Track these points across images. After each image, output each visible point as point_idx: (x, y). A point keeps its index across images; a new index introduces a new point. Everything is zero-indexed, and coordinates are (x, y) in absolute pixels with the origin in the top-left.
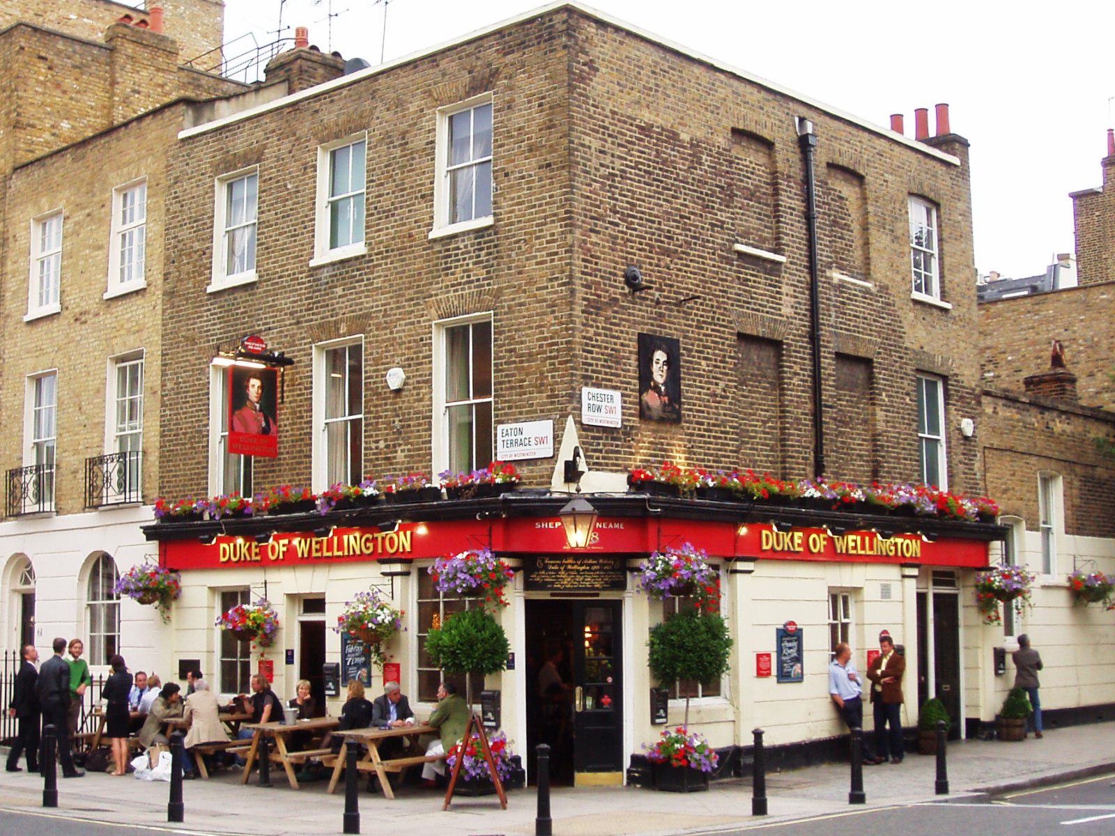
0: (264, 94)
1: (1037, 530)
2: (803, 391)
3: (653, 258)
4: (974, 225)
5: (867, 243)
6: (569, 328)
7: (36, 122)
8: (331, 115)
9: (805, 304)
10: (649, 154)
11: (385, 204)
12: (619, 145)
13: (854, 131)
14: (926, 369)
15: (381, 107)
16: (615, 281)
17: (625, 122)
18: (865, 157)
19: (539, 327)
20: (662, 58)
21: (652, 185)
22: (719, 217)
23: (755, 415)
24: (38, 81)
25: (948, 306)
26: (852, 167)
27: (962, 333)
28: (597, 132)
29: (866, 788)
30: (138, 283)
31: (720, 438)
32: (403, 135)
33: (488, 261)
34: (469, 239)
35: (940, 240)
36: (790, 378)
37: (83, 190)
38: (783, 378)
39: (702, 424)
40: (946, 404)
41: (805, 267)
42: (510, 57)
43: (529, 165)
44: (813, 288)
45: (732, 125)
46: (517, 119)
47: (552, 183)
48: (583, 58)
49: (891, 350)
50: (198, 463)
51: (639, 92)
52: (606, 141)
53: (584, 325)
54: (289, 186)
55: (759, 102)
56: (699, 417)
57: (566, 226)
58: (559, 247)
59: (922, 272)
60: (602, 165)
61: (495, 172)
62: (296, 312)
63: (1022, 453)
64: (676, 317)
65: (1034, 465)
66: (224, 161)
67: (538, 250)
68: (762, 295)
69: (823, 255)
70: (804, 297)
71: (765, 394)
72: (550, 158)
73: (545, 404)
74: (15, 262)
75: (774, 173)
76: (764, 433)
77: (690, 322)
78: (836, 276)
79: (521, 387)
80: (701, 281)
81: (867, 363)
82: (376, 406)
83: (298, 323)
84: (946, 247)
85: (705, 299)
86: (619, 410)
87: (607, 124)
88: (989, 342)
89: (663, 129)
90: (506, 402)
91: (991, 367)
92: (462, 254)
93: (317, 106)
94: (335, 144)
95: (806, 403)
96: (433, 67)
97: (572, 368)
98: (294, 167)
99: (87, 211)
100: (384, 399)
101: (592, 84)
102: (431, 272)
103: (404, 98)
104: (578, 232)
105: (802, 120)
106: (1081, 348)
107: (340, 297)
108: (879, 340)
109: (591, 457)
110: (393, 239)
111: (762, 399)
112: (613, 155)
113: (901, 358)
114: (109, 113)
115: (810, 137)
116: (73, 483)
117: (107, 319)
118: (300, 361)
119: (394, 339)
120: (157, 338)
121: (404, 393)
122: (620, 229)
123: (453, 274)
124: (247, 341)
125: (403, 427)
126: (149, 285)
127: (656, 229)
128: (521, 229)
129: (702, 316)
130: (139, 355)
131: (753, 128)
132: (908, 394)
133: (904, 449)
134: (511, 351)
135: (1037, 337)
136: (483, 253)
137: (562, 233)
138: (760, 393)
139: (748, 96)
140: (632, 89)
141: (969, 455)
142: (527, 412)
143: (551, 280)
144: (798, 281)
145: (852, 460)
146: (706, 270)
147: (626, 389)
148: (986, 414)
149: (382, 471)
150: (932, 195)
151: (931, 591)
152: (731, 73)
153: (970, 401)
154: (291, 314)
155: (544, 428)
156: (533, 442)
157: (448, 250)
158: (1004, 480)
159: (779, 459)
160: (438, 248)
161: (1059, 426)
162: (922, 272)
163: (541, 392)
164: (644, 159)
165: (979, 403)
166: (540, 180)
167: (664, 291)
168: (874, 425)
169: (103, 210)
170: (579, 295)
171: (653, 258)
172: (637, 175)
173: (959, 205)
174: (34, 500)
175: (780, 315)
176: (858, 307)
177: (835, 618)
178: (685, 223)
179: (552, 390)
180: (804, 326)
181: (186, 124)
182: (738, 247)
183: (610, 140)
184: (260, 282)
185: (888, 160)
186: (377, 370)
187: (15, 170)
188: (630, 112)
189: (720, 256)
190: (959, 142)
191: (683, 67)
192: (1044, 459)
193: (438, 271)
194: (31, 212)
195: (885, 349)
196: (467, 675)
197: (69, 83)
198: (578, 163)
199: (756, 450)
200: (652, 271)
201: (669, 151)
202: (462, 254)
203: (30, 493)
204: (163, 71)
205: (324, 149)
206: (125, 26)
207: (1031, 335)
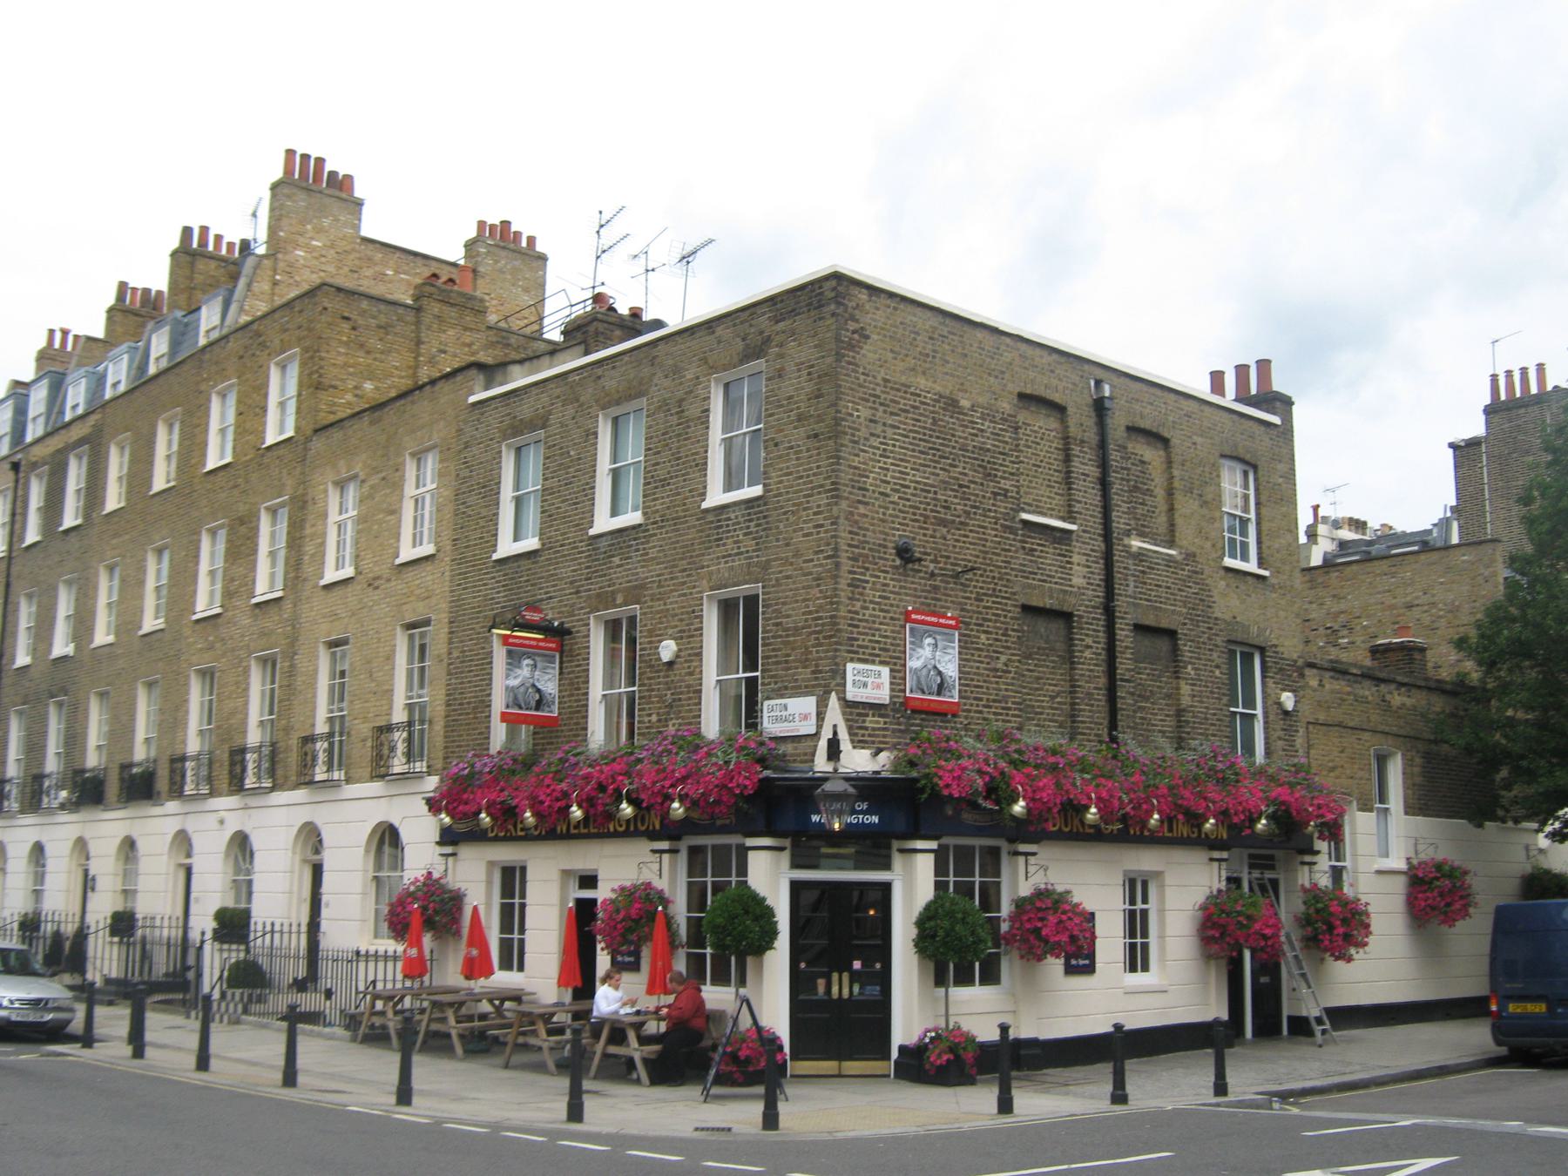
0: (560, 356)
1: (1371, 810)
2: (1096, 665)
4: (1298, 487)
5: (1171, 509)
6: (833, 603)
7: (338, 383)
8: (612, 381)
10: (925, 422)
11: (661, 473)
15: (660, 374)
17: (898, 390)
18: (1171, 418)
23: (1041, 689)
24: (340, 341)
25: (1266, 573)
26: (1155, 430)
27: (1283, 602)
28: (868, 401)
29: (1129, 1089)
30: (427, 549)
31: (1001, 714)
32: (681, 401)
33: (757, 532)
34: (740, 510)
35: (1258, 504)
38: (1074, 651)
39: (981, 699)
40: (1264, 677)
41: (1099, 535)
43: (797, 435)
45: (1018, 390)
46: (787, 387)
47: (819, 454)
48: (852, 326)
50: (480, 734)
52: (876, 409)
53: (850, 599)
54: (572, 453)
57: (832, 497)
58: (825, 519)
59: (1238, 537)
61: (765, 441)
63: (1352, 728)
64: (952, 589)
66: (512, 427)
67: (805, 522)
69: (1120, 521)
70: (1099, 567)
73: (809, 680)
74: (313, 526)
75: (1066, 439)
76: (1052, 708)
78: (1136, 543)
81: (1171, 634)
82: (650, 678)
83: (577, 592)
84: (1264, 511)
85: (985, 571)
86: (887, 686)
87: (878, 393)
88: (1343, 606)
89: (941, 396)
90: (772, 677)
91: (1345, 632)
92: (734, 524)
93: (599, 372)
94: (518, 440)
97: (836, 643)
99: (383, 474)
100: (657, 672)
101: (863, 352)
102: (704, 543)
104: (844, 504)
105: (1098, 383)
109: (856, 735)
110: (668, 508)
111: (1051, 673)
112: (884, 424)
113: (1210, 628)
114: (415, 373)
115: (1106, 401)
116: (362, 752)
117: (397, 586)
118: (578, 632)
120: (444, 606)
121: (676, 666)
123: (724, 545)
124: (526, 610)
125: (674, 700)
126: (438, 551)
129: (982, 588)
130: (427, 623)
131: (1040, 391)
132: (1218, 667)
134: (777, 624)
136: (752, 524)
137: (828, 504)
139: (1037, 359)
140: (907, 355)
141: (1290, 731)
142: (793, 688)
143: (817, 553)
144: (1092, 550)
146: (986, 540)
147: (895, 664)
148: (1311, 687)
150: (1248, 457)
152: (1017, 336)
153: (1290, 673)
154: (572, 583)
155: (808, 704)
156: (797, 719)
157: (719, 521)
158: (1331, 757)
161: (1397, 699)
162: (1238, 537)
163: (805, 667)
165: (1302, 675)
166: (808, 450)
167: (939, 562)
168: (1179, 700)
169: (397, 474)
170: (845, 568)
173: (1279, 466)
174: (404, 760)
177: (1133, 902)
178: (964, 493)
179: (817, 666)
181: (477, 388)
182: (1025, 516)
183: (881, 408)
186: (650, 642)
187: (316, 431)
189: (1002, 525)
190: (1281, 401)
192: (1379, 735)
193: (710, 541)
194: (331, 476)
195: (1192, 620)
196: (733, 958)
197: (374, 343)
198: (846, 434)
201: (947, 418)
202: (734, 524)
203: (320, 761)
205: (605, 416)
206: (433, 286)
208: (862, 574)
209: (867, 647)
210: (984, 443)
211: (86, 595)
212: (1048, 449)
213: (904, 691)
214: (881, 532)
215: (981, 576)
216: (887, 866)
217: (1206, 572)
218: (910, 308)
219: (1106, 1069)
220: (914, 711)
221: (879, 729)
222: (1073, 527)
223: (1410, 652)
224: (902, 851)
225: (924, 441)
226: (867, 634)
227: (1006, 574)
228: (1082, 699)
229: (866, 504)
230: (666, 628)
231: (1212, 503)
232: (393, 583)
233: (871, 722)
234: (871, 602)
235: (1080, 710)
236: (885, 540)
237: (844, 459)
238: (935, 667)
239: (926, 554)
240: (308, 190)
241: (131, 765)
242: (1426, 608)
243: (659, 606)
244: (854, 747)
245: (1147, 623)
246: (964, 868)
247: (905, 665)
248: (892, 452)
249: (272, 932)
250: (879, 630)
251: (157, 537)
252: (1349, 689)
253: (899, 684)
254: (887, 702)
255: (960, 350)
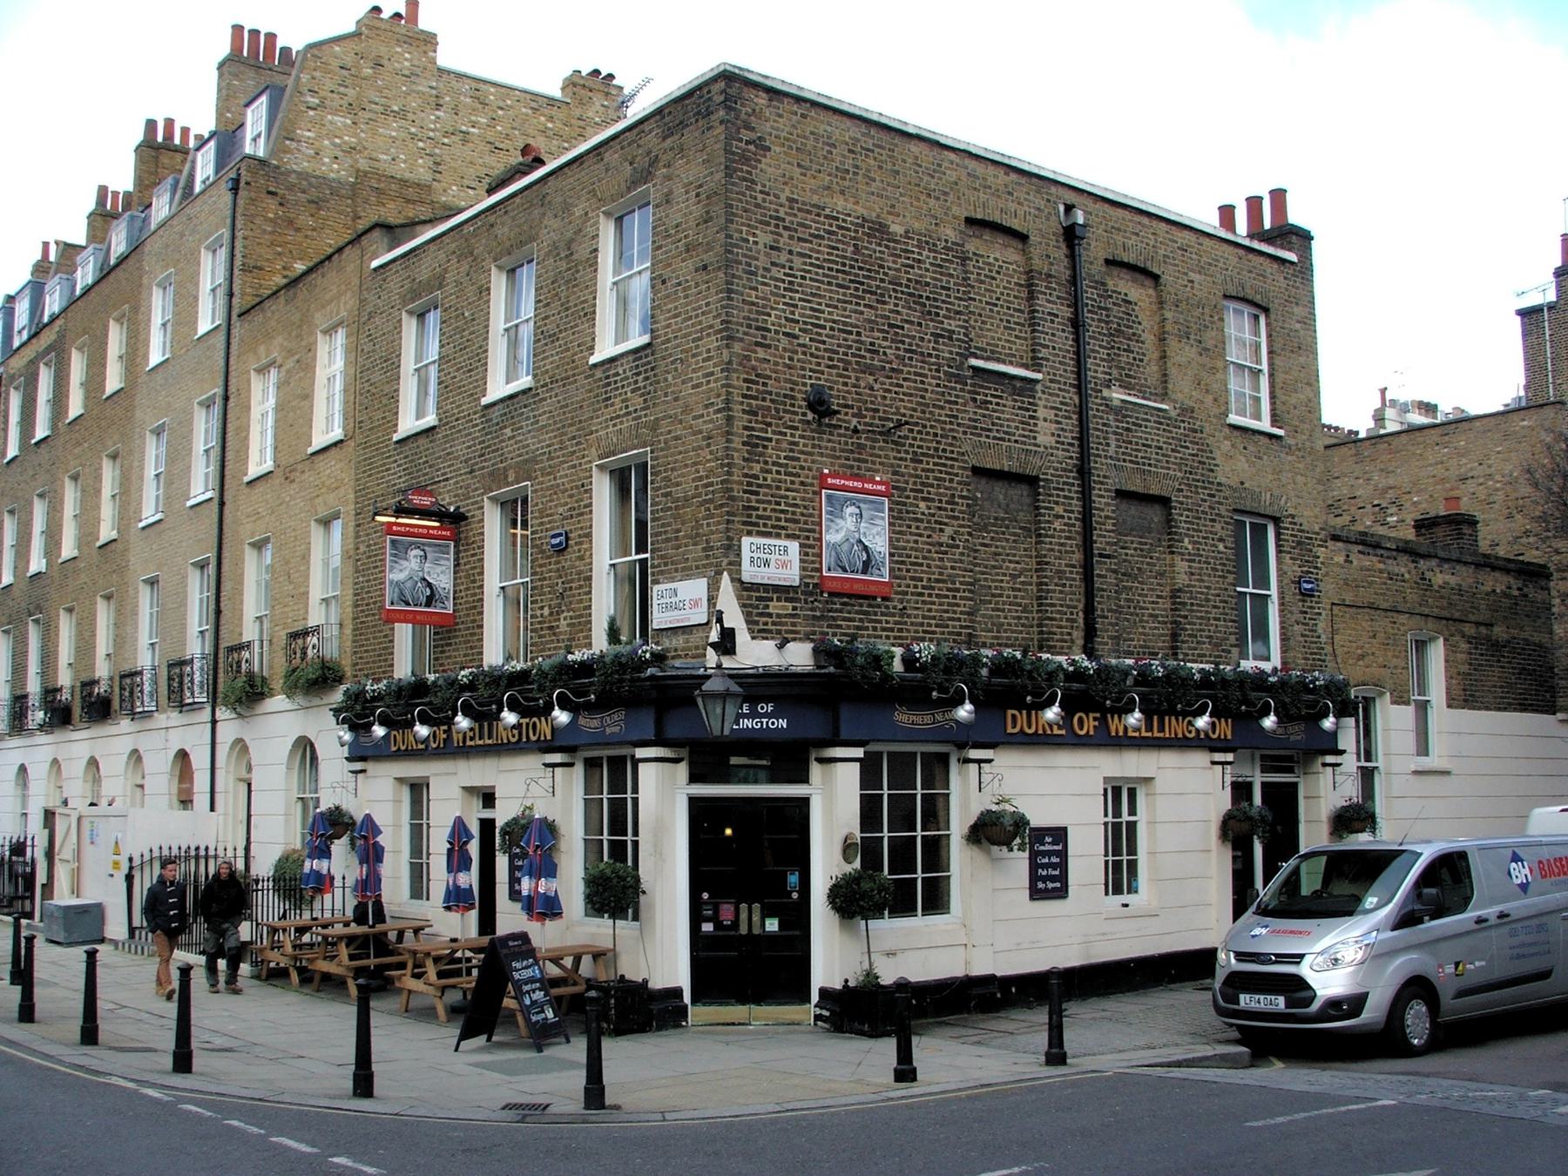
1: (1407, 703)
3: (849, 378)
4: (1319, 335)
5: (1163, 357)
9: (1072, 431)
10: (844, 250)
11: (551, 328)
12: (800, 239)
13: (1146, 221)
14: (1248, 509)
16: (793, 405)
17: (809, 212)
18: (1162, 252)
19: (695, 464)
20: (864, 135)
21: (849, 288)
22: (945, 326)
25: (1281, 432)
28: (768, 224)
33: (645, 387)
35: (1270, 352)
36: (1049, 522)
37: (294, 333)
40: (1279, 552)
42: (669, 141)
44: (1082, 412)
45: (966, 214)
48: (746, 135)
49: (1196, 487)
51: (829, 175)
53: (745, 460)
54: (466, 314)
55: (1006, 186)
56: (916, 571)
58: (715, 365)
60: (773, 264)
62: (470, 459)
64: (881, 449)
65: (1403, 625)
66: (412, 290)
67: (694, 371)
68: (1008, 420)
69: (1096, 369)
71: (1014, 541)
72: (709, 257)
76: (1014, 589)
77: (903, 455)
78: (1117, 395)
79: (677, 538)
80: (919, 404)
81: (1164, 502)
82: (541, 566)
83: (471, 472)
85: (924, 426)
86: (796, 564)
87: (782, 214)
88: (1391, 482)
91: (1393, 510)
92: (622, 380)
93: (492, 219)
95: (1073, 552)
96: (598, 162)
98: (470, 291)
99: (297, 357)
103: (570, 201)
105: (1069, 208)
106: (1498, 485)
107: (509, 439)
108: (1179, 474)
109: (757, 623)
112: (790, 252)
118: (473, 516)
119: (558, 485)
122: (801, 341)
123: (612, 405)
127: (853, 341)
128: (678, 346)
129: (920, 447)
132: (1221, 540)
133: (1215, 607)
134: (666, 495)
135: (1447, 473)
136: (640, 378)
138: (1007, 540)
143: (707, 406)
144: (1062, 403)
145: (1141, 621)
146: (926, 390)
149: (547, 642)
150: (1258, 298)
151: (1258, 779)
157: (608, 377)
159: (1035, 622)
160: (599, 374)
163: (695, 544)
164: (837, 256)
169: (310, 354)
171: (849, 378)
172: (827, 276)
173: (1296, 310)
175: (1036, 445)
176: (1151, 433)
177: (1117, 813)
178: (897, 333)
180: (1071, 458)
182: (974, 362)
183: (786, 234)
184: (439, 426)
185: (1194, 256)
188: (815, 199)
189: (946, 373)
190: (1297, 235)
191: (896, 145)
197: (306, 220)
199: (1003, 610)
200: (848, 392)
202: (622, 380)
204: (414, 202)
205: (500, 268)
207: (1439, 471)
208: (761, 430)
209: (769, 518)
210: (921, 276)
211: (54, 509)
212: (1007, 285)
213: (820, 570)
214: (786, 381)
215: (920, 432)
216: (804, 779)
217: (1206, 430)
218: (823, 115)
219: (1041, 1016)
220: (830, 594)
221: (786, 616)
222: (1039, 376)
223: (1461, 523)
224: (821, 761)
225: (844, 272)
226: (769, 502)
227: (952, 430)
228: (1051, 578)
229: (769, 346)
230: (556, 506)
231: (1214, 352)
232: (307, 475)
233: (775, 607)
234: (774, 464)
235: (1048, 591)
236: (792, 390)
237: (737, 292)
238: (860, 541)
239: (846, 406)
240: (258, 67)
241: (94, 682)
242: (1481, 480)
243: (548, 481)
244: (753, 638)
245: (1133, 488)
246: (901, 776)
247: (820, 540)
248: (800, 285)
249: (197, 857)
250: (787, 497)
251: (110, 443)
252: (1382, 566)
253: (813, 562)
254: (797, 583)
255: (889, 166)
